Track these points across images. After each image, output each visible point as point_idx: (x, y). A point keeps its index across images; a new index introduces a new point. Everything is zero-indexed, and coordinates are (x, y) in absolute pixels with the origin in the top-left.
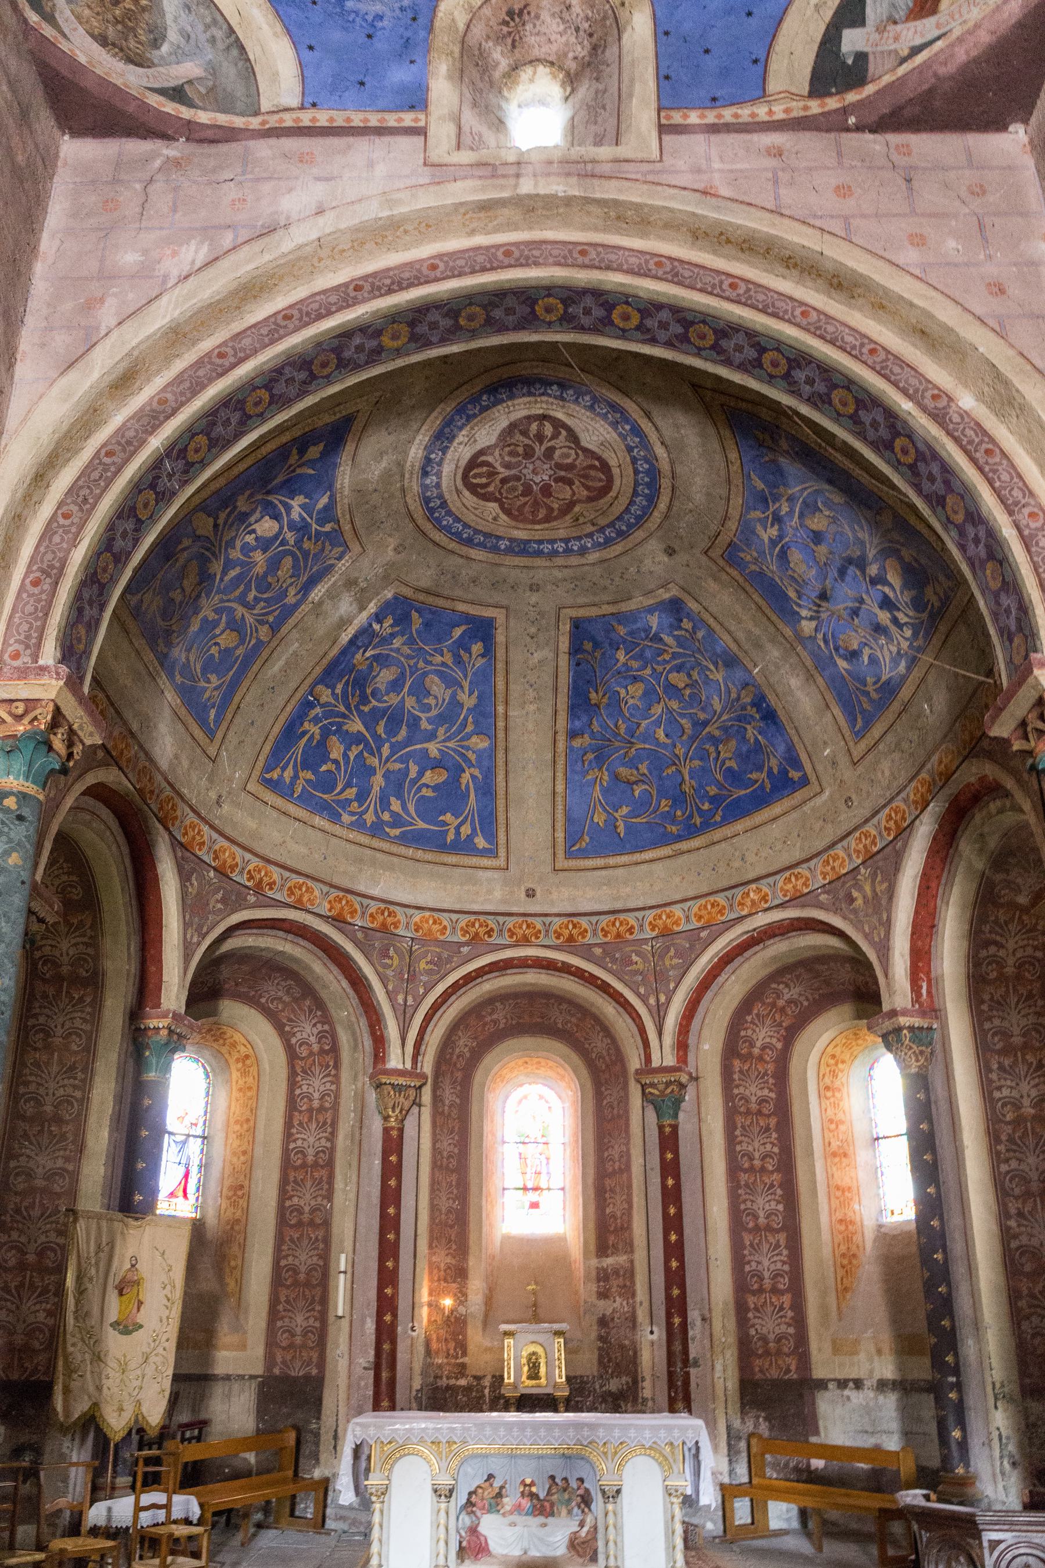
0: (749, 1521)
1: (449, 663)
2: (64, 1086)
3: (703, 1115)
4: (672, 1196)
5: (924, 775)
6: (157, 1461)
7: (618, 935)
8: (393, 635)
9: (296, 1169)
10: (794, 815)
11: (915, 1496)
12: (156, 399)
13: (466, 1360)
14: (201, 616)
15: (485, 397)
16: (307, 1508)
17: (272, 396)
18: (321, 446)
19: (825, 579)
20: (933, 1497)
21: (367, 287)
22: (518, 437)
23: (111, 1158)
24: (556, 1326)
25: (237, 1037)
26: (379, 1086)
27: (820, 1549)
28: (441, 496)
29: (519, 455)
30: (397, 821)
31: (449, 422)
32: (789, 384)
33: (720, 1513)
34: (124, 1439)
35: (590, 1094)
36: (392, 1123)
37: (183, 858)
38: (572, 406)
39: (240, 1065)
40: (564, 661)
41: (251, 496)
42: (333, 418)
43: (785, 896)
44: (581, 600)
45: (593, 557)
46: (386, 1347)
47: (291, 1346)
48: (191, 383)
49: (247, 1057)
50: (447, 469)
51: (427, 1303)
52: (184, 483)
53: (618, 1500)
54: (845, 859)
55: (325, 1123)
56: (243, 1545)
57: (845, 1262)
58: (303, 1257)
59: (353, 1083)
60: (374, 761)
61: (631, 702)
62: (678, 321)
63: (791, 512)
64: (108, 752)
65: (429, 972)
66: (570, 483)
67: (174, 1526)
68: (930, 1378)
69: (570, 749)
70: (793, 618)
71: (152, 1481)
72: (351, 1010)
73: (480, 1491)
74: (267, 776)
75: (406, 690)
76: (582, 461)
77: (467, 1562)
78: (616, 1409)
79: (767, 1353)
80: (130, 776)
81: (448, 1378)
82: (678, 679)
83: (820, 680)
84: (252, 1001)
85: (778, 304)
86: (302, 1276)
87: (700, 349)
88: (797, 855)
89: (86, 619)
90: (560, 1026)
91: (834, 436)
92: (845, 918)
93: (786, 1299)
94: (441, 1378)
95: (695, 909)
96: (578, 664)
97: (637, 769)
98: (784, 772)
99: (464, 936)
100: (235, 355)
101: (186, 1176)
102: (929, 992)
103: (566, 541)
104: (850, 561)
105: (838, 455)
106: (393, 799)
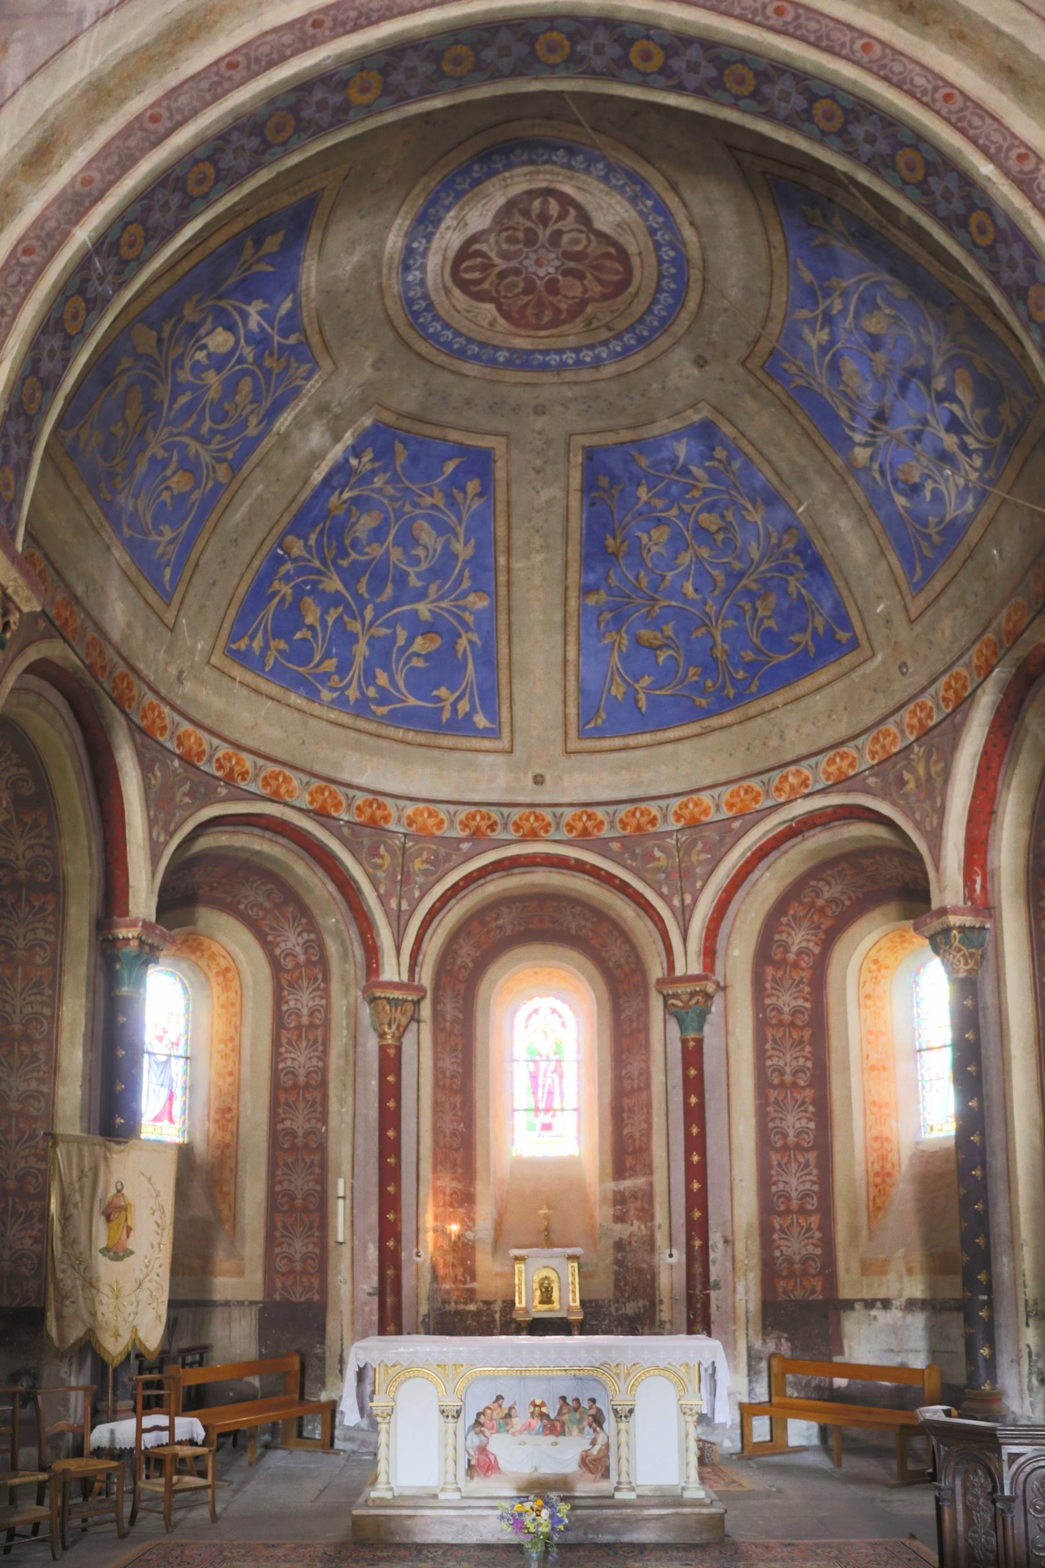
0: (768, 1438)
1: (442, 506)
2: (31, 1003)
3: (731, 1027)
4: (695, 1115)
5: (990, 635)
6: (159, 1385)
7: (639, 828)
8: (373, 473)
9: (286, 1090)
10: (839, 686)
11: (936, 1412)
12: (79, 179)
13: (475, 1285)
14: (149, 453)
15: (476, 167)
16: (315, 1430)
17: (218, 171)
18: (280, 236)
19: (884, 393)
20: (954, 1412)
21: (328, 23)
22: (518, 219)
23: (88, 1082)
24: (570, 1251)
25: (216, 948)
26: (373, 1000)
27: (839, 1464)
28: (426, 296)
29: (518, 242)
30: (384, 698)
31: (433, 201)
32: (846, 142)
33: (738, 1431)
34: (122, 1364)
35: (607, 1007)
36: (389, 1040)
37: (143, 745)
38: (583, 177)
39: (221, 979)
40: (575, 500)
41: (199, 302)
42: (294, 199)
43: (828, 779)
44: (596, 424)
45: (609, 370)
46: (390, 1272)
47: (291, 1272)
48: (119, 156)
49: (227, 970)
50: (433, 262)
51: (431, 1231)
52: (120, 286)
53: (631, 1419)
54: (899, 735)
55: (316, 1041)
56: (250, 1464)
57: (879, 1180)
58: (299, 1182)
59: (344, 998)
60: (356, 626)
61: (654, 549)
62: (711, 61)
63: (844, 312)
64: (51, 622)
65: (425, 873)
66: (580, 276)
67: (178, 1447)
68: (959, 1296)
69: (583, 608)
70: (845, 444)
71: (153, 1404)
72: (340, 918)
73: (488, 1412)
74: (234, 647)
75: (391, 538)
76: (595, 248)
77: (476, 1479)
78: (633, 1332)
79: (792, 1274)
80: (78, 649)
81: (456, 1303)
82: (710, 521)
83: (875, 522)
84: (231, 909)
85: (835, 35)
86: (299, 1202)
87: (737, 98)
88: (843, 730)
89: (13, 460)
90: (573, 932)
91: (897, 210)
92: (894, 804)
93: (814, 1220)
94: (449, 1303)
95: (725, 797)
96: (592, 504)
97: (662, 631)
98: (830, 633)
99: (678, 820)
100: (171, 118)
101: (171, 1097)
102: (984, 887)
103: (577, 350)
104: (913, 372)
105: (903, 237)
106: (378, 671)
